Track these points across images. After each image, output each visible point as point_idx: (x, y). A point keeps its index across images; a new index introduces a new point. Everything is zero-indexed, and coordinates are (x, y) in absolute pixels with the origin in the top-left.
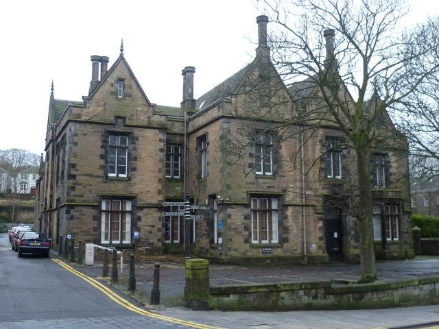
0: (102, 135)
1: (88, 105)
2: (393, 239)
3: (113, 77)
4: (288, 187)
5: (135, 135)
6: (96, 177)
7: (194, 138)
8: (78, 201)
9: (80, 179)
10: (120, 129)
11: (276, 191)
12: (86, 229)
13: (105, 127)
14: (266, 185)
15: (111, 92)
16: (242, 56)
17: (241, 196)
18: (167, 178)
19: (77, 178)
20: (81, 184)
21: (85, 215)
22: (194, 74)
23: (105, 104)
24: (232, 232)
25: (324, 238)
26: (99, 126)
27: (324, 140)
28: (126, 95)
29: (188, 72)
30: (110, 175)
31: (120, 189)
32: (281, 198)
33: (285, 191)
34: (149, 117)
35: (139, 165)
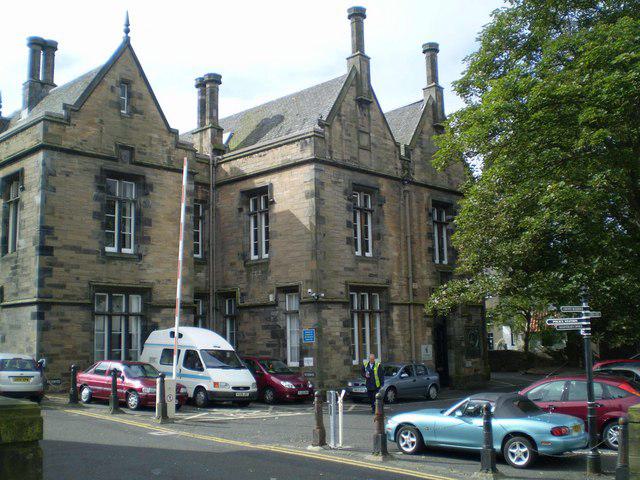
0: (96, 177)
1: (73, 121)
2: (119, 249)
3: (123, 80)
4: (392, 275)
5: (148, 181)
6: (87, 252)
7: (234, 192)
8: (58, 293)
9: (61, 255)
10: (125, 167)
11: (378, 282)
12: (70, 346)
13: (100, 163)
14: (368, 273)
15: (111, 101)
16: (332, 64)
17: (338, 289)
18: (195, 258)
19: (55, 252)
20: (62, 265)
21: (68, 321)
22: (220, 86)
23: (101, 121)
24: (329, 349)
25: (567, 379)
26: (92, 160)
27: (431, 207)
28: (134, 111)
29: (42, 49)
30: (108, 249)
31: (125, 275)
32: (384, 293)
33: (389, 282)
34: (169, 152)
35: (153, 232)
